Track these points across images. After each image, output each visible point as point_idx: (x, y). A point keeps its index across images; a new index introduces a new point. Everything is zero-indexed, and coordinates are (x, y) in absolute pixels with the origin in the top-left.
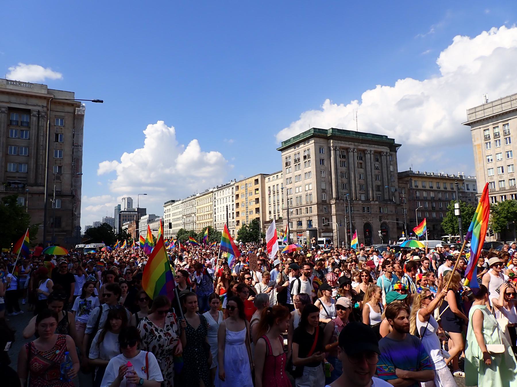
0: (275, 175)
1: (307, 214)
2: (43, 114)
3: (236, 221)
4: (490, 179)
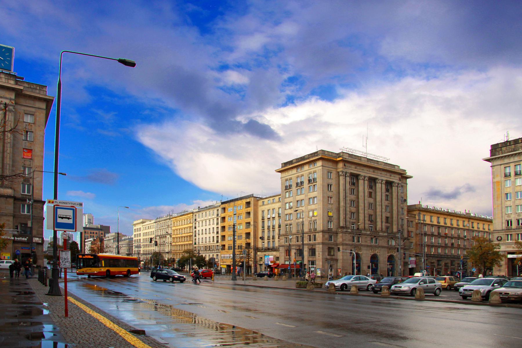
0: (271, 199)
1: (297, 243)
2: (11, 108)
3: (221, 245)
4: (507, 217)
